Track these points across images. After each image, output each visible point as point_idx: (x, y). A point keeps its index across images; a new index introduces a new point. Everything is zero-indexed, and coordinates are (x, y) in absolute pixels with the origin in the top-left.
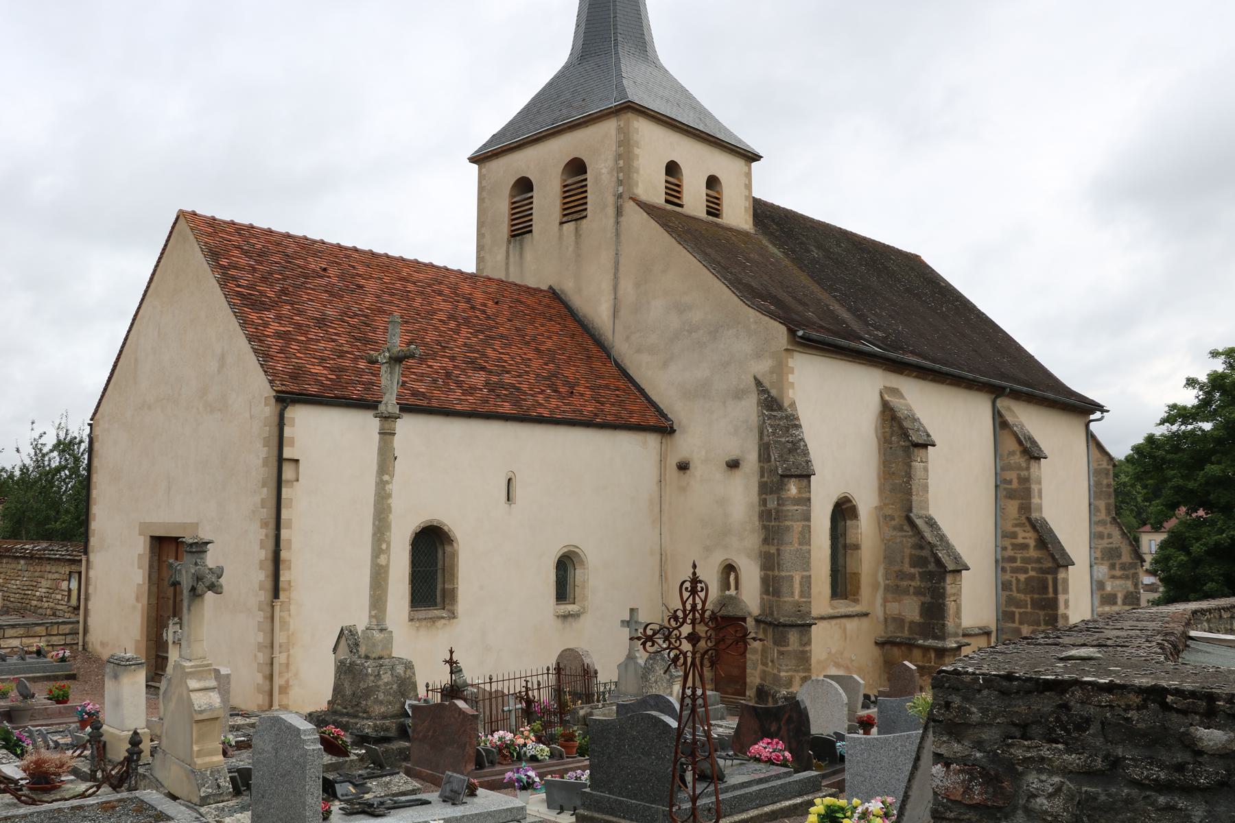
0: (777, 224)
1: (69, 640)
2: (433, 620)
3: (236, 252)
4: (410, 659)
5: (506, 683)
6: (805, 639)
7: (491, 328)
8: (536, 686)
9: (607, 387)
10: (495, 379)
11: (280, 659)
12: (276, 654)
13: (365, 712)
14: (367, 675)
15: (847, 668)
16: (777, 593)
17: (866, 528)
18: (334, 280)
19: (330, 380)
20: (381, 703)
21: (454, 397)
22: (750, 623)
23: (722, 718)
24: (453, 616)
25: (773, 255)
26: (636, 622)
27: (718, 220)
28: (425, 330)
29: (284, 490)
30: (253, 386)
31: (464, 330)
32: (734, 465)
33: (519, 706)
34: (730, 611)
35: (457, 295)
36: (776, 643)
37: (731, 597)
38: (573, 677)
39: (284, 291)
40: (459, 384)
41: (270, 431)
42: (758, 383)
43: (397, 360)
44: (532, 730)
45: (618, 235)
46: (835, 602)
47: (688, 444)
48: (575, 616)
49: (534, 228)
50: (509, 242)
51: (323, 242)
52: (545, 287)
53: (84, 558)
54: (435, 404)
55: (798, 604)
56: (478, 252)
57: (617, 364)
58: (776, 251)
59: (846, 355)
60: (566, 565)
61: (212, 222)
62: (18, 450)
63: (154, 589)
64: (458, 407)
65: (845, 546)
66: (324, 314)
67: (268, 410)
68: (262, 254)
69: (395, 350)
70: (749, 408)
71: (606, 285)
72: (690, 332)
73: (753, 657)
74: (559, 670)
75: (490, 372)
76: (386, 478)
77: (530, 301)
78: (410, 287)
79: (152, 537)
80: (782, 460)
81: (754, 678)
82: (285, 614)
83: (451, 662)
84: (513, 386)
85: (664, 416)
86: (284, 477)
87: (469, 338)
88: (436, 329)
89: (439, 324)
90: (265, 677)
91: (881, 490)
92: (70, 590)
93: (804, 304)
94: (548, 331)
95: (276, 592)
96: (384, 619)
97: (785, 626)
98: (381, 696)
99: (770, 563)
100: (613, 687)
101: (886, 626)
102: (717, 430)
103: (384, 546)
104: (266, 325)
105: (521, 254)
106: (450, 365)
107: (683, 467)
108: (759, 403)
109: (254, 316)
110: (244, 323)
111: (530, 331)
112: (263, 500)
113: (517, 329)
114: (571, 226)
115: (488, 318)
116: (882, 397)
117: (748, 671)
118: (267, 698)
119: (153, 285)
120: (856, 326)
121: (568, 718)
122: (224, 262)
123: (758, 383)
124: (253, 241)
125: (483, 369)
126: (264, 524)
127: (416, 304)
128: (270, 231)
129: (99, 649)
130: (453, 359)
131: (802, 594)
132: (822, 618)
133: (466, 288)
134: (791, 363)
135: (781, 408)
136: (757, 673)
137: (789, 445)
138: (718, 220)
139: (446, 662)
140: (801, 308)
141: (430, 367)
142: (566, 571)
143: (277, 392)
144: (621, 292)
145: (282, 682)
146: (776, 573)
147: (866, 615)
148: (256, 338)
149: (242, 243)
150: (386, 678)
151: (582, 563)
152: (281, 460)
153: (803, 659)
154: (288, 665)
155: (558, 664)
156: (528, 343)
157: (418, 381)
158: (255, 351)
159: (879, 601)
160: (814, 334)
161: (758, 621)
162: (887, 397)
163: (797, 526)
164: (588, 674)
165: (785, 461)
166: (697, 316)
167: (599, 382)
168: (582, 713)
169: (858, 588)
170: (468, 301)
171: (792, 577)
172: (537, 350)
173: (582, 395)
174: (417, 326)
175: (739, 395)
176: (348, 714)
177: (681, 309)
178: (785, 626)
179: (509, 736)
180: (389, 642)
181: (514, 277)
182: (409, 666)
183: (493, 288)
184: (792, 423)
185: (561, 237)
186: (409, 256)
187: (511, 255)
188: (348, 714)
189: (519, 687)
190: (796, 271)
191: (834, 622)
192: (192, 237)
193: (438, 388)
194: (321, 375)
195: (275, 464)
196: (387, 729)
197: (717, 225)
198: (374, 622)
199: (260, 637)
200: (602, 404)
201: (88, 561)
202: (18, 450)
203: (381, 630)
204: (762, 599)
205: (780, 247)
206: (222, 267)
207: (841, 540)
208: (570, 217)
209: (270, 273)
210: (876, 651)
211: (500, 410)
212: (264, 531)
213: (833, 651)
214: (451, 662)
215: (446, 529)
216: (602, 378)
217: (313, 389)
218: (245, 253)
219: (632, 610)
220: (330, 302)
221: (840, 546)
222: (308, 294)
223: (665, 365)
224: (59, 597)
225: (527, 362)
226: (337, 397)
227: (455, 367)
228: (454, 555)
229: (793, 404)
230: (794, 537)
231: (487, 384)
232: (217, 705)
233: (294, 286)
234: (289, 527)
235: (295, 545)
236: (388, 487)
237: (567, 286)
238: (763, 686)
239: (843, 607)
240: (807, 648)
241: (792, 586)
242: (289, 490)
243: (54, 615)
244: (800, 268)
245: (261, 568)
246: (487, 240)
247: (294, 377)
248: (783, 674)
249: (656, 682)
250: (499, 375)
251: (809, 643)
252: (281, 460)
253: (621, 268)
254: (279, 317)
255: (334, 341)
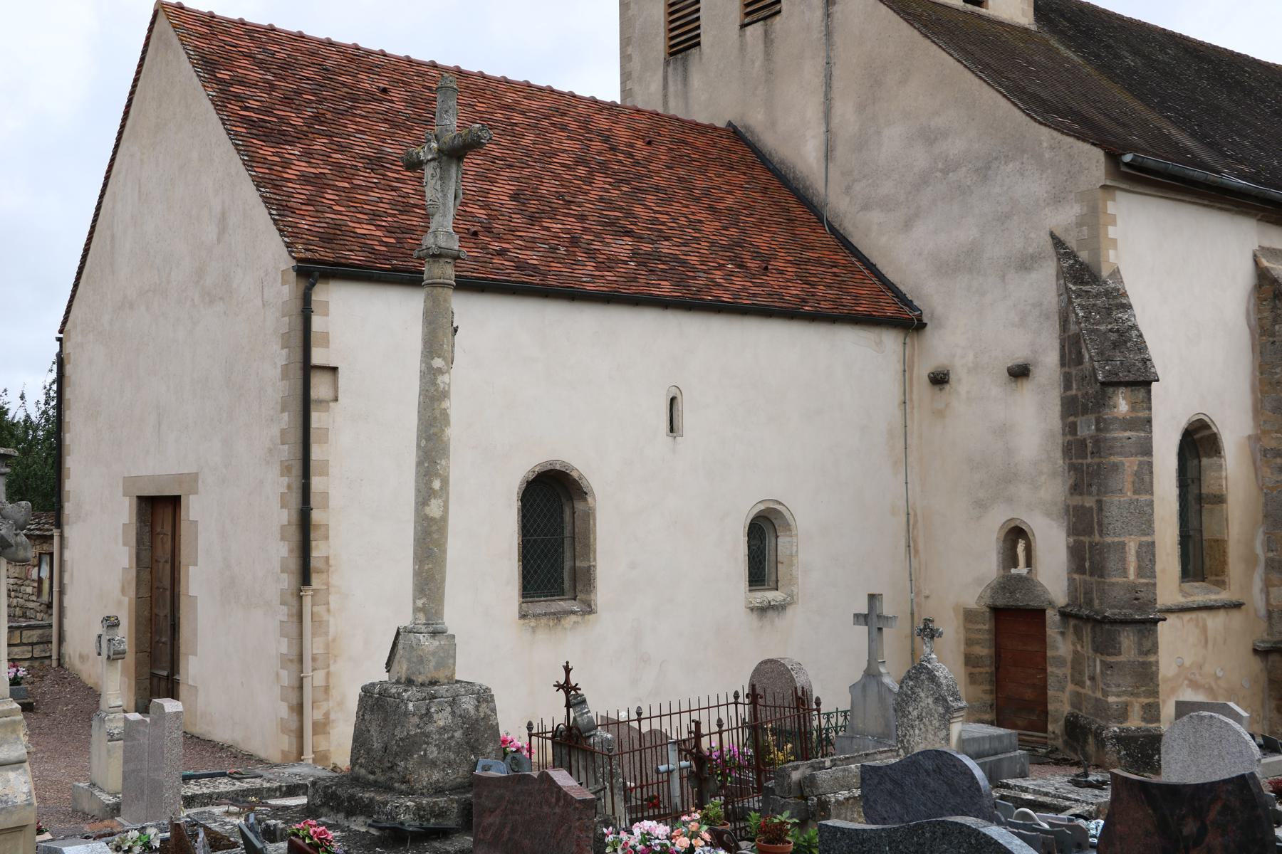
0: (1068, 20)
1: (37, 652)
2: (558, 616)
3: (244, 62)
4: (486, 684)
5: (666, 720)
6: (1148, 644)
7: (641, 177)
8: (715, 728)
9: (818, 261)
10: (647, 247)
11: (315, 679)
12: (307, 671)
13: (404, 781)
14: (406, 714)
15: (1210, 690)
16: (1098, 570)
17: (1234, 469)
18: (399, 106)
19: (386, 244)
20: (433, 764)
21: (585, 273)
22: (1052, 617)
23: (1023, 775)
24: (589, 609)
25: (1067, 59)
26: (880, 617)
27: (982, 11)
28: (540, 178)
29: (315, 417)
30: (266, 254)
31: (599, 180)
32: (1020, 373)
33: (684, 763)
34: (1021, 600)
35: (589, 131)
36: (1098, 649)
37: (1020, 578)
38: (779, 711)
39: (318, 118)
40: (591, 254)
41: (289, 323)
42: (1058, 242)
43: (454, 154)
44: (706, 819)
45: (829, 33)
46: (1187, 586)
47: (947, 342)
48: (780, 608)
49: (703, 38)
50: (667, 63)
51: (383, 54)
52: (721, 124)
53: (56, 533)
54: (552, 281)
55: (1134, 588)
56: (623, 83)
57: (834, 231)
58: (1071, 55)
59: (1201, 195)
60: (763, 531)
61: (210, 20)
62: (22, 397)
63: (146, 575)
64: (590, 287)
65: (1200, 498)
66: (380, 151)
67: (285, 291)
68: (285, 66)
69: (447, 137)
70: (1043, 284)
71: (812, 110)
72: (946, 172)
73: (1059, 672)
74: (754, 696)
75: (640, 238)
76: (438, 363)
77: (700, 142)
78: (517, 118)
79: (139, 497)
80: (1100, 361)
81: (1060, 703)
82: (320, 609)
83: (567, 687)
84: (675, 258)
85: (909, 304)
86: (314, 394)
87: (607, 191)
88: (557, 176)
89: (560, 170)
90: (291, 708)
91: (1257, 411)
92: (40, 580)
93: (1124, 125)
94: (727, 183)
95: (305, 575)
96: (439, 613)
97: (1115, 624)
98: (433, 753)
99: (1085, 526)
100: (841, 720)
101: (1271, 625)
102: (994, 319)
103: (436, 484)
104: (286, 164)
105: (685, 70)
106: (578, 227)
107: (939, 379)
108: (1061, 273)
109: (267, 151)
110: (251, 161)
111: (700, 183)
112: (283, 432)
113: (681, 180)
114: (757, 29)
115: (637, 163)
116: (1256, 262)
117: (1050, 693)
118: (294, 741)
119: (129, 123)
120: (1205, 155)
121: (771, 784)
122: (224, 75)
123: (1058, 242)
124: (275, 48)
125: (628, 233)
126: (286, 470)
127: (525, 142)
128: (301, 36)
129: (77, 664)
130: (582, 218)
131: (1140, 572)
132: (1170, 611)
133: (602, 122)
134: (1111, 208)
135: (1096, 279)
136: (1066, 697)
137: (1113, 336)
138: (982, 11)
139: (559, 686)
140: (1120, 130)
141: (547, 229)
142: (762, 539)
143: (299, 260)
144: (835, 121)
145: (318, 715)
146: (1097, 538)
147: (1238, 606)
148: (270, 185)
149: (255, 51)
150: (442, 719)
151: (787, 527)
152: (308, 368)
153: (1146, 676)
154: (327, 689)
155: (753, 687)
156: (698, 199)
157: (527, 248)
158: (266, 201)
159: (1257, 584)
160: (1151, 161)
161: (1065, 615)
162: (1265, 263)
163: (1130, 464)
164: (802, 702)
165: (1108, 360)
166: (955, 146)
167: (807, 254)
168: (796, 776)
169: (1224, 563)
170: (606, 139)
171: (1123, 545)
172: (712, 210)
173: (782, 272)
174: (526, 172)
175: (1026, 263)
176: (376, 785)
177: (929, 137)
178: (1114, 622)
179: (661, 830)
180: (448, 656)
181: (675, 108)
182: (484, 696)
183: (643, 123)
184: (1116, 302)
185: (743, 48)
186: (516, 76)
187: (671, 83)
188: (376, 785)
189: (678, 728)
190: (1105, 82)
191: (1187, 617)
192: (176, 41)
193: (559, 260)
194: (372, 237)
195: (299, 374)
196: (442, 814)
197: (980, 16)
198: (422, 618)
199: (284, 647)
200: (813, 285)
201: (62, 536)
202: (22, 397)
203: (435, 634)
204: (1071, 581)
205: (1078, 49)
206: (221, 81)
207: (1193, 490)
208: (755, 16)
209: (298, 93)
210: (1256, 664)
211: (656, 292)
212: (285, 480)
213: (1187, 663)
214: (567, 687)
215: (575, 474)
216: (812, 249)
217: (357, 257)
218: (260, 64)
219: (872, 597)
220: (391, 135)
221: (1191, 497)
222: (356, 123)
223: (907, 225)
224: (29, 590)
225: (696, 224)
226: (395, 269)
227: (585, 230)
228: (589, 515)
229: (1116, 273)
230: (1126, 480)
231: (635, 254)
232: (21, 799)
233: (335, 111)
234: (324, 472)
235: (336, 499)
236: (443, 379)
237: (755, 119)
238: (1077, 717)
239: (1200, 594)
240: (1152, 659)
241: (1123, 560)
242: (324, 415)
243: (24, 616)
244: (1111, 79)
245: (282, 539)
246: (636, 64)
247: (327, 239)
248: (1111, 699)
249: (920, 718)
250: (653, 242)
251: (1154, 649)
252: (308, 368)
253: (837, 84)
254: (308, 155)
255: (394, 189)
